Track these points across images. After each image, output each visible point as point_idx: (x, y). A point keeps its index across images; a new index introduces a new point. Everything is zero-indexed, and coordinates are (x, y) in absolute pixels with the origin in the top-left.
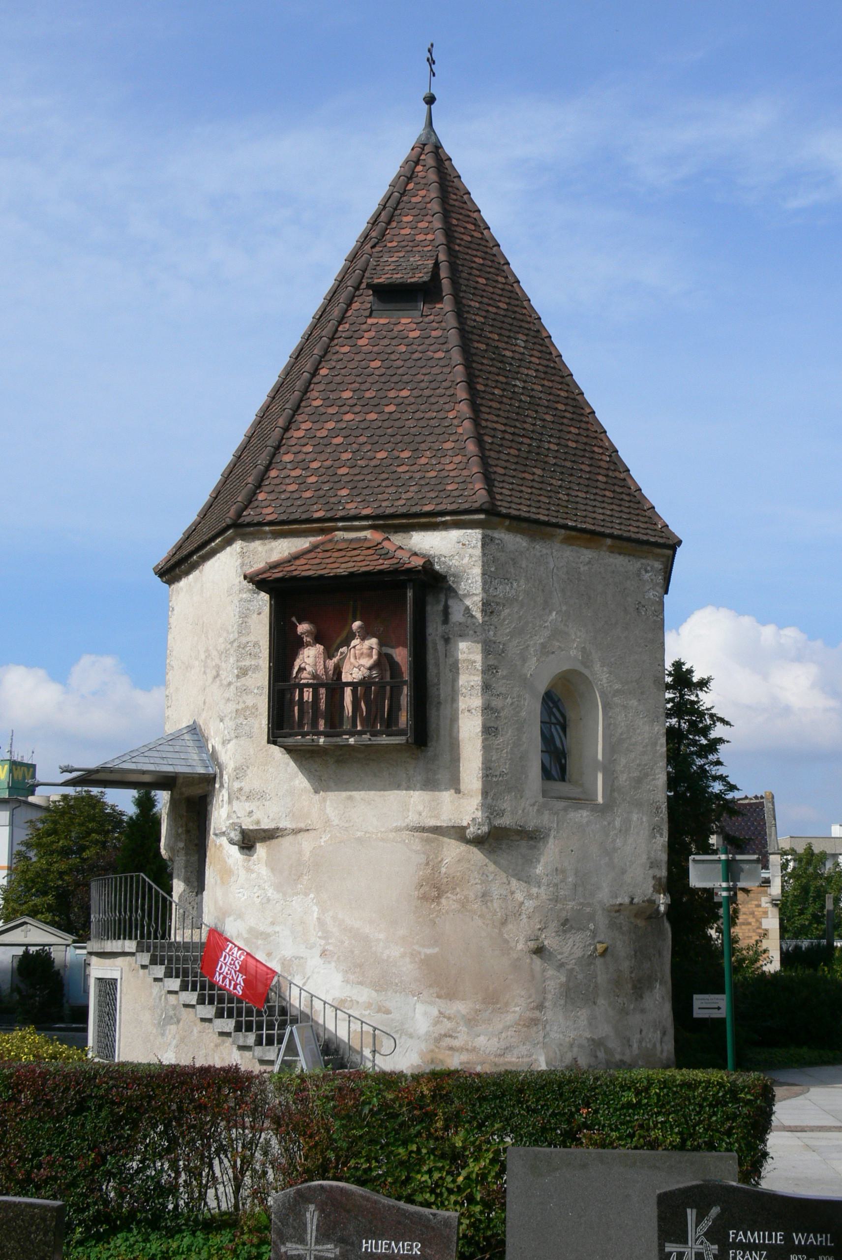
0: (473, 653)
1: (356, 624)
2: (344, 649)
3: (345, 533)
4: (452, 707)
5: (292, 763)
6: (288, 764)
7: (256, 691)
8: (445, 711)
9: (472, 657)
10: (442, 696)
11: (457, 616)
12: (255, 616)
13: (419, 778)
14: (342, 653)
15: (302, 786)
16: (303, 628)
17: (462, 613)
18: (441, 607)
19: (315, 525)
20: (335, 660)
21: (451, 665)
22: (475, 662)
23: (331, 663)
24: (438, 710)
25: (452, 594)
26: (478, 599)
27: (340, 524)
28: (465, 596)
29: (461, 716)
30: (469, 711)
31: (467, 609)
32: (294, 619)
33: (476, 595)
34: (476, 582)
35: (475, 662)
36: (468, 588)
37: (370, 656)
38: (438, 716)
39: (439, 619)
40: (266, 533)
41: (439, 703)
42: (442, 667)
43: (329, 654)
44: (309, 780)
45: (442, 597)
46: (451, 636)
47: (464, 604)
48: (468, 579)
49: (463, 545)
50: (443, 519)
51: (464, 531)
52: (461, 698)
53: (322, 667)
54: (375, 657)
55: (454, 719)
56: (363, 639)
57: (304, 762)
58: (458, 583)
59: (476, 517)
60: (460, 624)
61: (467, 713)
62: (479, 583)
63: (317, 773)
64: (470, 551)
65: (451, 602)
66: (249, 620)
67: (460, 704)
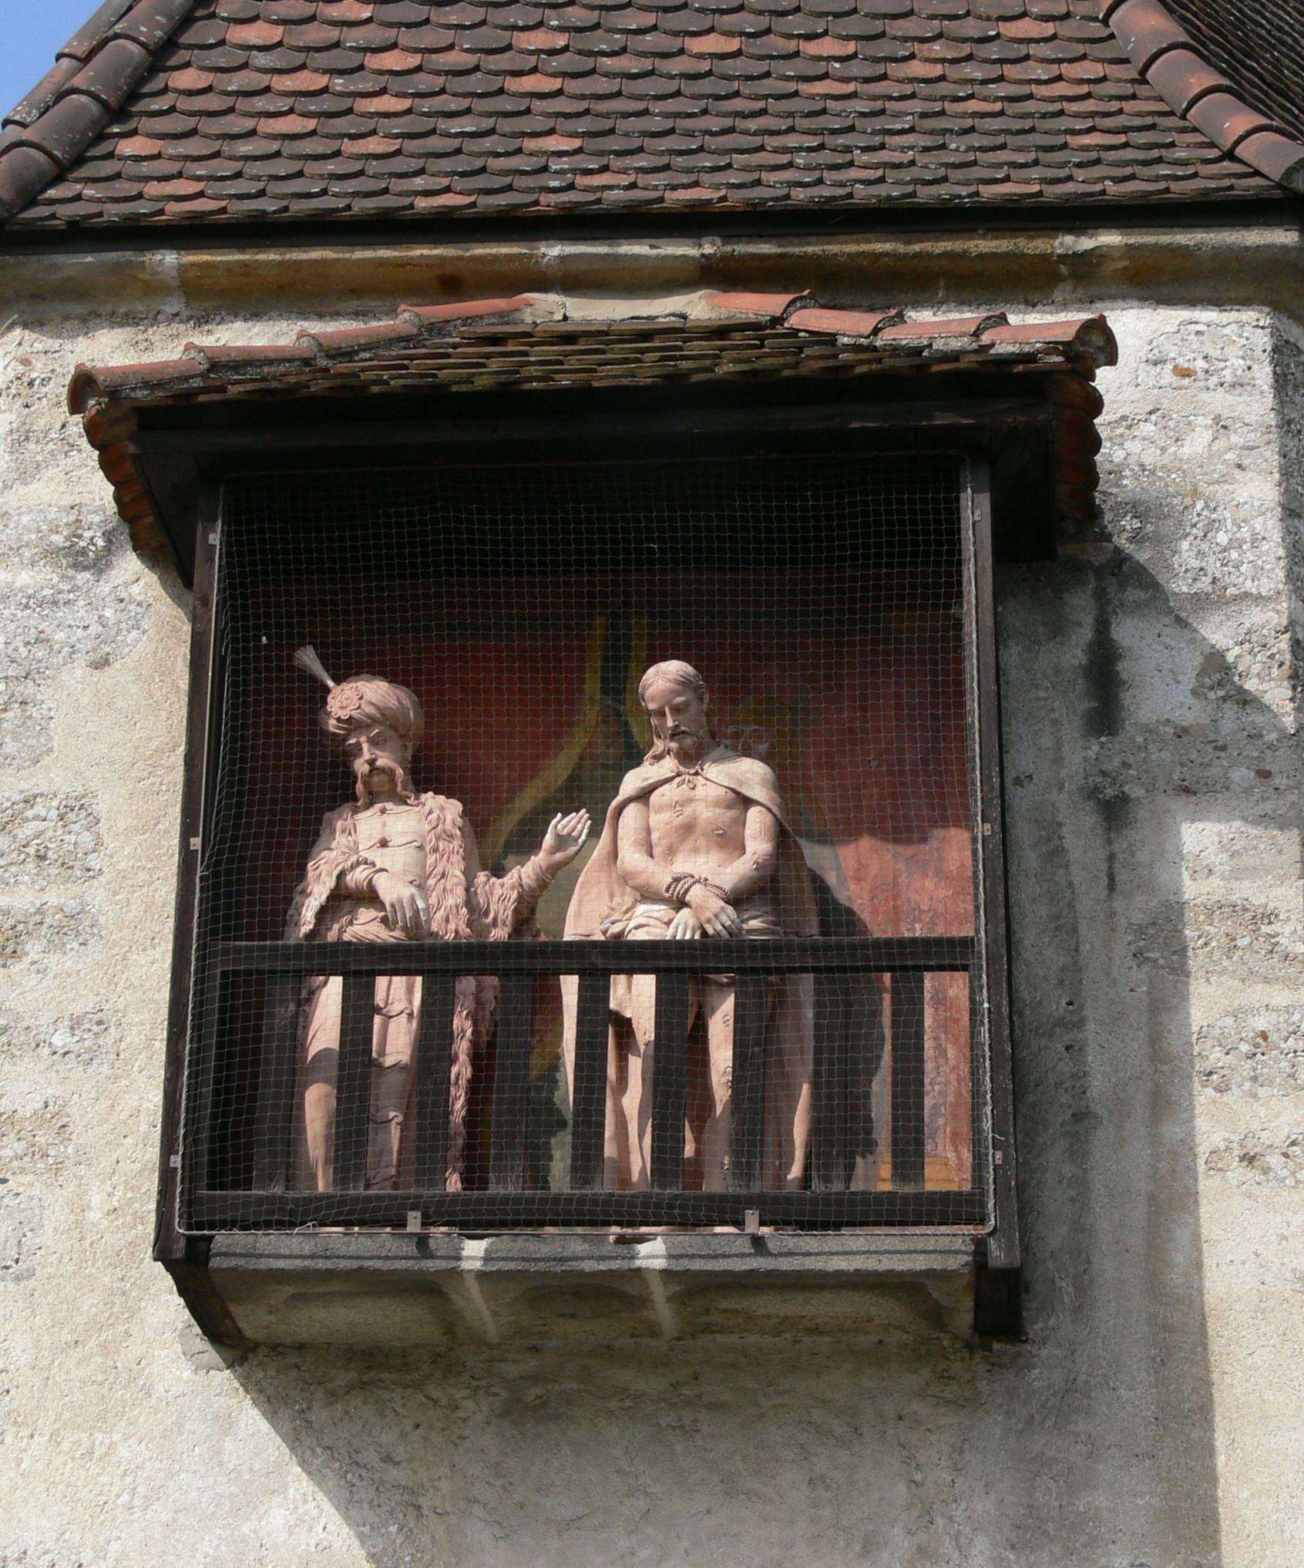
0: (1252, 872)
1: (663, 677)
2: (573, 823)
3: (570, 301)
4: (1155, 1139)
5: (252, 1419)
6: (227, 1424)
7: (60, 1039)
8: (1119, 1159)
9: (1252, 892)
10: (1098, 1085)
11: (1161, 690)
12: (79, 672)
13: (983, 1505)
14: (562, 841)
15: (307, 1541)
16: (357, 697)
17: (1189, 680)
18: (1075, 651)
19: (419, 252)
20: (526, 872)
21: (1140, 930)
22: (1270, 917)
23: (501, 894)
24: (1078, 1151)
25: (1133, 594)
26: (1269, 618)
27: (553, 251)
28: (1201, 602)
29: (1207, 1185)
30: (1249, 1159)
31: (1216, 666)
32: (308, 658)
33: (1258, 599)
34: (1256, 540)
35: (1270, 917)
36: (1213, 566)
37: (731, 841)
38: (1081, 1184)
39: (1071, 707)
40: (155, 289)
41: (1082, 1116)
42: (1090, 938)
43: (493, 840)
44: (347, 1507)
45: (1081, 607)
46: (1136, 791)
47: (1195, 640)
48: (1212, 526)
49: (1184, 373)
50: (1086, 243)
51: (1184, 314)
52: (1204, 1097)
53: (457, 896)
54: (758, 844)
55: (1171, 1198)
56: (691, 758)
57: (320, 1415)
58: (1164, 543)
59: (1254, 237)
60: (1182, 732)
61: (1237, 1172)
62: (1274, 547)
63: (393, 1474)
64: (1220, 401)
65: (1126, 632)
66: (45, 694)
67: (1201, 1124)
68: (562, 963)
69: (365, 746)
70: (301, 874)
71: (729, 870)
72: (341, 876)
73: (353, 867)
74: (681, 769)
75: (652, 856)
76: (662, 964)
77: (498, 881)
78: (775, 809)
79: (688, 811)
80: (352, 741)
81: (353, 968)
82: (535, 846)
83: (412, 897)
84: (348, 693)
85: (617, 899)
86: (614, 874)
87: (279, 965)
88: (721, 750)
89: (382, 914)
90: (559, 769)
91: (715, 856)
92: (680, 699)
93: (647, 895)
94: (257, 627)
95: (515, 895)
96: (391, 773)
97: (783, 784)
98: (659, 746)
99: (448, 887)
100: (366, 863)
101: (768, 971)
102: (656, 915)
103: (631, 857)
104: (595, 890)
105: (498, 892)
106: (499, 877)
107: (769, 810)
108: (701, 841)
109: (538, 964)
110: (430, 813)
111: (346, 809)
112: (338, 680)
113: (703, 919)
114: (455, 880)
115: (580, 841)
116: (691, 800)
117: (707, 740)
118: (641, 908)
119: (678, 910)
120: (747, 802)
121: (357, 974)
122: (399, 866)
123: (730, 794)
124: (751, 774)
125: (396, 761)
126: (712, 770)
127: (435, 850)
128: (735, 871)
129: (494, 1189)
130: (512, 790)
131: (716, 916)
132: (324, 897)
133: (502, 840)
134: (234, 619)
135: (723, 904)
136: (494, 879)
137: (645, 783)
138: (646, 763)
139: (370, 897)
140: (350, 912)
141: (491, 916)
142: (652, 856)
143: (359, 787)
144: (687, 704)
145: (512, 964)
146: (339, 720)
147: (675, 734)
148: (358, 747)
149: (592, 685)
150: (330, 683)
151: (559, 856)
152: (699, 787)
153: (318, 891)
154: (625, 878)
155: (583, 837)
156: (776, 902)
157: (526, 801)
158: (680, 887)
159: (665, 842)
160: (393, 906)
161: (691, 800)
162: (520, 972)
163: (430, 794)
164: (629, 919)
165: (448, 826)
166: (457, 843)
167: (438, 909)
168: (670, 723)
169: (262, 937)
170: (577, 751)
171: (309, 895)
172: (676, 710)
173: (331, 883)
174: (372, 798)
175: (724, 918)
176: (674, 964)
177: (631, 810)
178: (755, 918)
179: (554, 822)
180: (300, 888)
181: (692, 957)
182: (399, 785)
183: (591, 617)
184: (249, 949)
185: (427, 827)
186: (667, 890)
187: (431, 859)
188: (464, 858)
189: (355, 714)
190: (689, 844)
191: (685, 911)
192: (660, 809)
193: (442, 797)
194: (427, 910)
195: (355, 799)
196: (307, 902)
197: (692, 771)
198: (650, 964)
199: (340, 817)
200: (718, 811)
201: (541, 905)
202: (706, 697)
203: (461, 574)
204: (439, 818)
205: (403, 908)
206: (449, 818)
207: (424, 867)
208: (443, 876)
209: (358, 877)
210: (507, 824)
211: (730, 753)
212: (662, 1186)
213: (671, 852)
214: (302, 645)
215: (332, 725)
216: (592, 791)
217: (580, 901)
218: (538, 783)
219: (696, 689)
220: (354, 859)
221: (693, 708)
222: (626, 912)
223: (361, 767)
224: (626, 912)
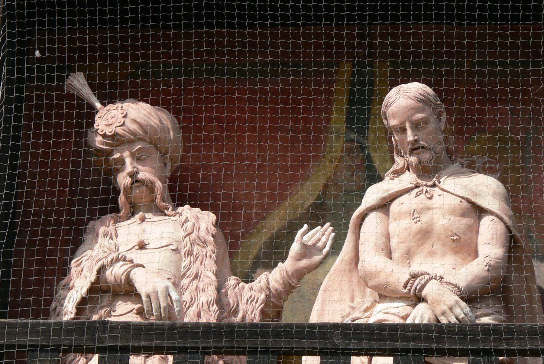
1: (403, 98)
14: (307, 251)
16: (120, 118)
20: (274, 277)
32: (79, 83)
37: (465, 246)
43: (244, 246)
53: (210, 294)
54: (490, 243)
56: (428, 171)
68: (306, 344)
69: (128, 161)
70: (65, 272)
71: (463, 270)
72: (101, 271)
73: (112, 263)
74: (420, 181)
75: (391, 259)
77: (247, 286)
78: (506, 219)
79: (425, 218)
80: (117, 156)
81: (108, 344)
82: (283, 257)
83: (167, 289)
84: (113, 113)
85: (358, 299)
86: (355, 278)
87: (39, 340)
88: (457, 166)
89: (137, 306)
90: (306, 194)
91: (450, 260)
92: (420, 116)
93: (385, 294)
94: (31, 43)
95: (262, 297)
96: (150, 187)
97: (514, 196)
98: (399, 162)
99: (201, 286)
100: (125, 260)
101: (500, 353)
102: (395, 311)
103: (372, 259)
104: (336, 296)
105: (247, 294)
106: (247, 282)
107: (501, 219)
108: (438, 247)
109: (283, 344)
110: (186, 221)
111: (109, 218)
112: (104, 104)
113: (438, 311)
114: (207, 281)
115: (325, 251)
116: (429, 209)
117: (444, 155)
118: (380, 307)
119: (414, 306)
120: (480, 212)
121: (113, 349)
122: (156, 266)
124: (486, 188)
125: (155, 175)
126: (448, 182)
127: (189, 254)
128: (470, 272)
131: (451, 309)
132: (85, 290)
133: (250, 261)
134: (11, 35)
135: (457, 298)
136: (242, 284)
137: (385, 194)
138: (387, 179)
139: (128, 290)
140: (107, 306)
141: (240, 315)
142: (391, 259)
143: (122, 198)
144: (426, 121)
145: (259, 343)
146: (104, 136)
147: (415, 149)
148: (122, 161)
149: (338, 121)
150: (98, 105)
151: (304, 263)
152: (436, 197)
153: (80, 280)
154: (365, 281)
155: (327, 248)
156: (507, 300)
157: (274, 223)
158: (418, 283)
159: (403, 248)
160: (148, 296)
161: (429, 209)
162: (264, 352)
163: (187, 207)
165: (202, 234)
166: (210, 248)
167: (191, 305)
168: (410, 137)
169: (24, 315)
171: (70, 289)
172: (417, 126)
173: (92, 277)
174: (133, 210)
175: (458, 311)
176: (411, 345)
177: (373, 218)
178: (487, 315)
179: (300, 232)
180: (63, 282)
181: (428, 339)
182: (158, 197)
183: (338, 64)
184: (11, 326)
185: (183, 234)
186: (405, 286)
187: (186, 262)
188: (216, 262)
189: (119, 130)
190: (426, 248)
191: (422, 305)
192: (400, 216)
193: (198, 209)
194: (180, 301)
195: (116, 210)
196: (69, 295)
197: (430, 183)
199: (103, 224)
200: (452, 218)
201: (287, 306)
202: (444, 117)
203: (220, 25)
204: (194, 226)
205: (158, 299)
206: (203, 227)
207: (178, 267)
208: (197, 276)
209: (116, 272)
210: (257, 242)
211: (465, 170)
213: (409, 255)
214: (72, 70)
215: (98, 142)
216: (337, 209)
217: (323, 303)
220: (114, 255)
221: (432, 126)
222: (366, 310)
223: (123, 180)
224: (366, 310)
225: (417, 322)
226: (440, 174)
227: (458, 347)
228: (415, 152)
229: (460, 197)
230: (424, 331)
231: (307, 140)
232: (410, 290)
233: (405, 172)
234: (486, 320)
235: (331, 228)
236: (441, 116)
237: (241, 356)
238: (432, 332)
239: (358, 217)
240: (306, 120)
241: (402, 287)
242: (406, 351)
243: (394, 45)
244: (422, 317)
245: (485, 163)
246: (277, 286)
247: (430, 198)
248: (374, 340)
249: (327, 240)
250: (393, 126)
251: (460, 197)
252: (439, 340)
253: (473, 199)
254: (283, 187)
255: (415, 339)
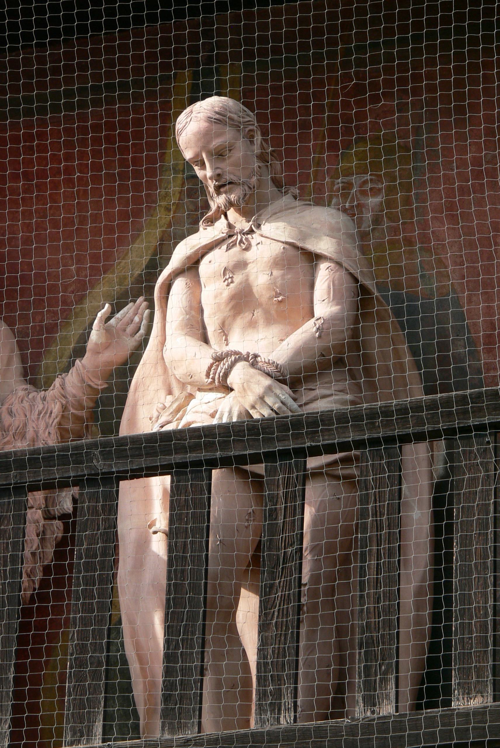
76: (175, 458)
95: (56, 409)
108: (258, 313)
120: (313, 259)
123: (292, 252)
124: (325, 231)
129: (460, 703)
130: (82, 286)
138: (201, 229)
164: (181, 419)
170: (158, 232)
172: (219, 155)
175: (269, 400)
177: (180, 286)
181: (210, 446)
186: (208, 375)
198: (160, 460)
202: (258, 138)
212: (172, 731)
213: (224, 330)
218: (113, 276)
219: (236, 126)
225: (225, 420)
226: (260, 216)
227: (247, 452)
228: (222, 190)
229: (283, 242)
230: (205, 436)
231: (137, 188)
232: (213, 379)
233: (220, 217)
234: (321, 406)
235: (145, 303)
236: (253, 137)
237: (35, 493)
238: (214, 436)
239: (161, 287)
240: (136, 161)
241: (204, 377)
242: (183, 465)
243: (249, 42)
244: (230, 412)
245: (365, 182)
246: (74, 392)
247: (247, 249)
248: (140, 456)
249: (141, 320)
250: (190, 159)
251: (283, 242)
252: (225, 445)
253: (300, 244)
254: (108, 256)
255: (195, 448)
